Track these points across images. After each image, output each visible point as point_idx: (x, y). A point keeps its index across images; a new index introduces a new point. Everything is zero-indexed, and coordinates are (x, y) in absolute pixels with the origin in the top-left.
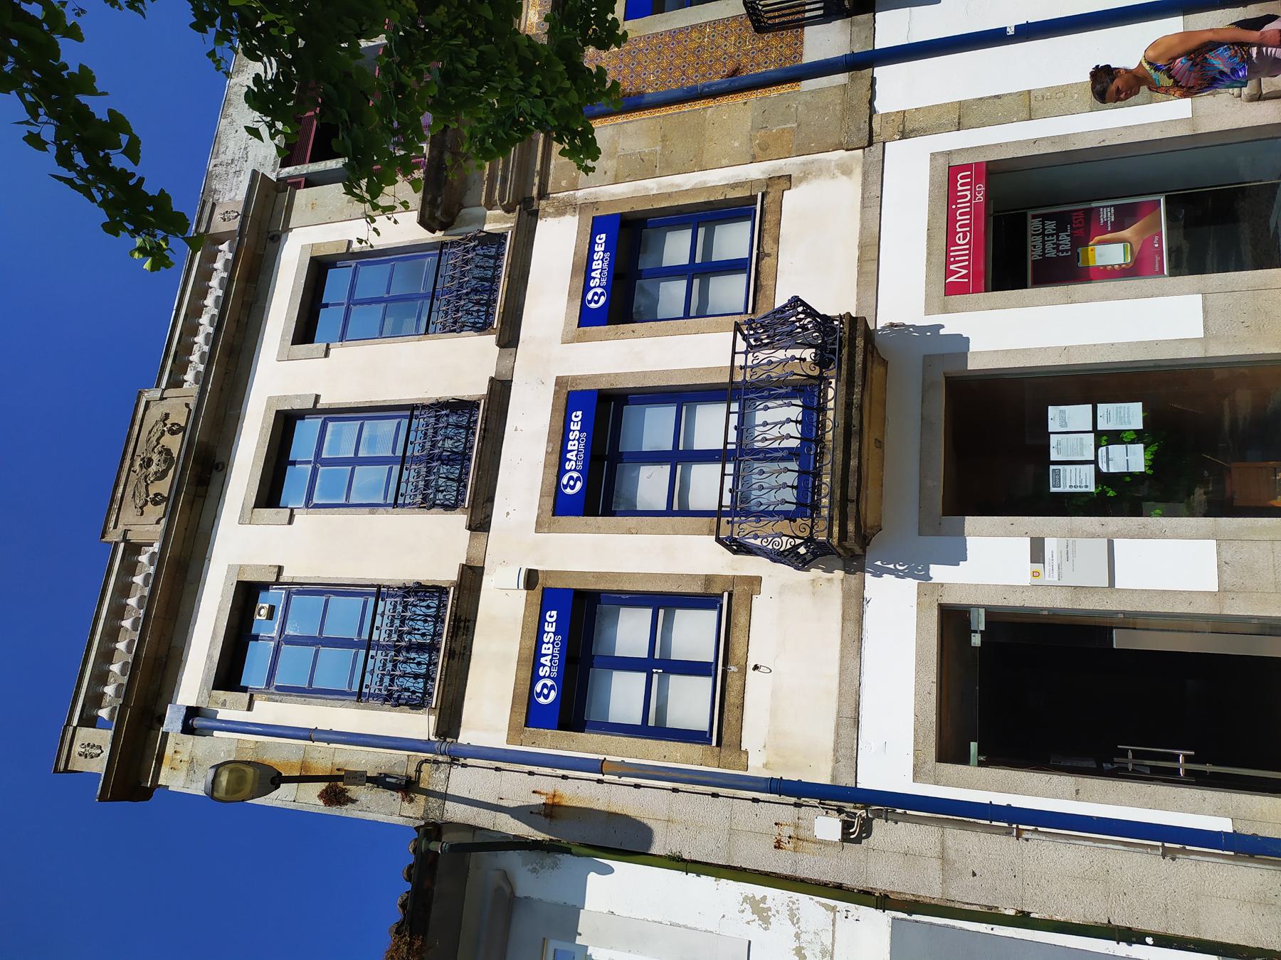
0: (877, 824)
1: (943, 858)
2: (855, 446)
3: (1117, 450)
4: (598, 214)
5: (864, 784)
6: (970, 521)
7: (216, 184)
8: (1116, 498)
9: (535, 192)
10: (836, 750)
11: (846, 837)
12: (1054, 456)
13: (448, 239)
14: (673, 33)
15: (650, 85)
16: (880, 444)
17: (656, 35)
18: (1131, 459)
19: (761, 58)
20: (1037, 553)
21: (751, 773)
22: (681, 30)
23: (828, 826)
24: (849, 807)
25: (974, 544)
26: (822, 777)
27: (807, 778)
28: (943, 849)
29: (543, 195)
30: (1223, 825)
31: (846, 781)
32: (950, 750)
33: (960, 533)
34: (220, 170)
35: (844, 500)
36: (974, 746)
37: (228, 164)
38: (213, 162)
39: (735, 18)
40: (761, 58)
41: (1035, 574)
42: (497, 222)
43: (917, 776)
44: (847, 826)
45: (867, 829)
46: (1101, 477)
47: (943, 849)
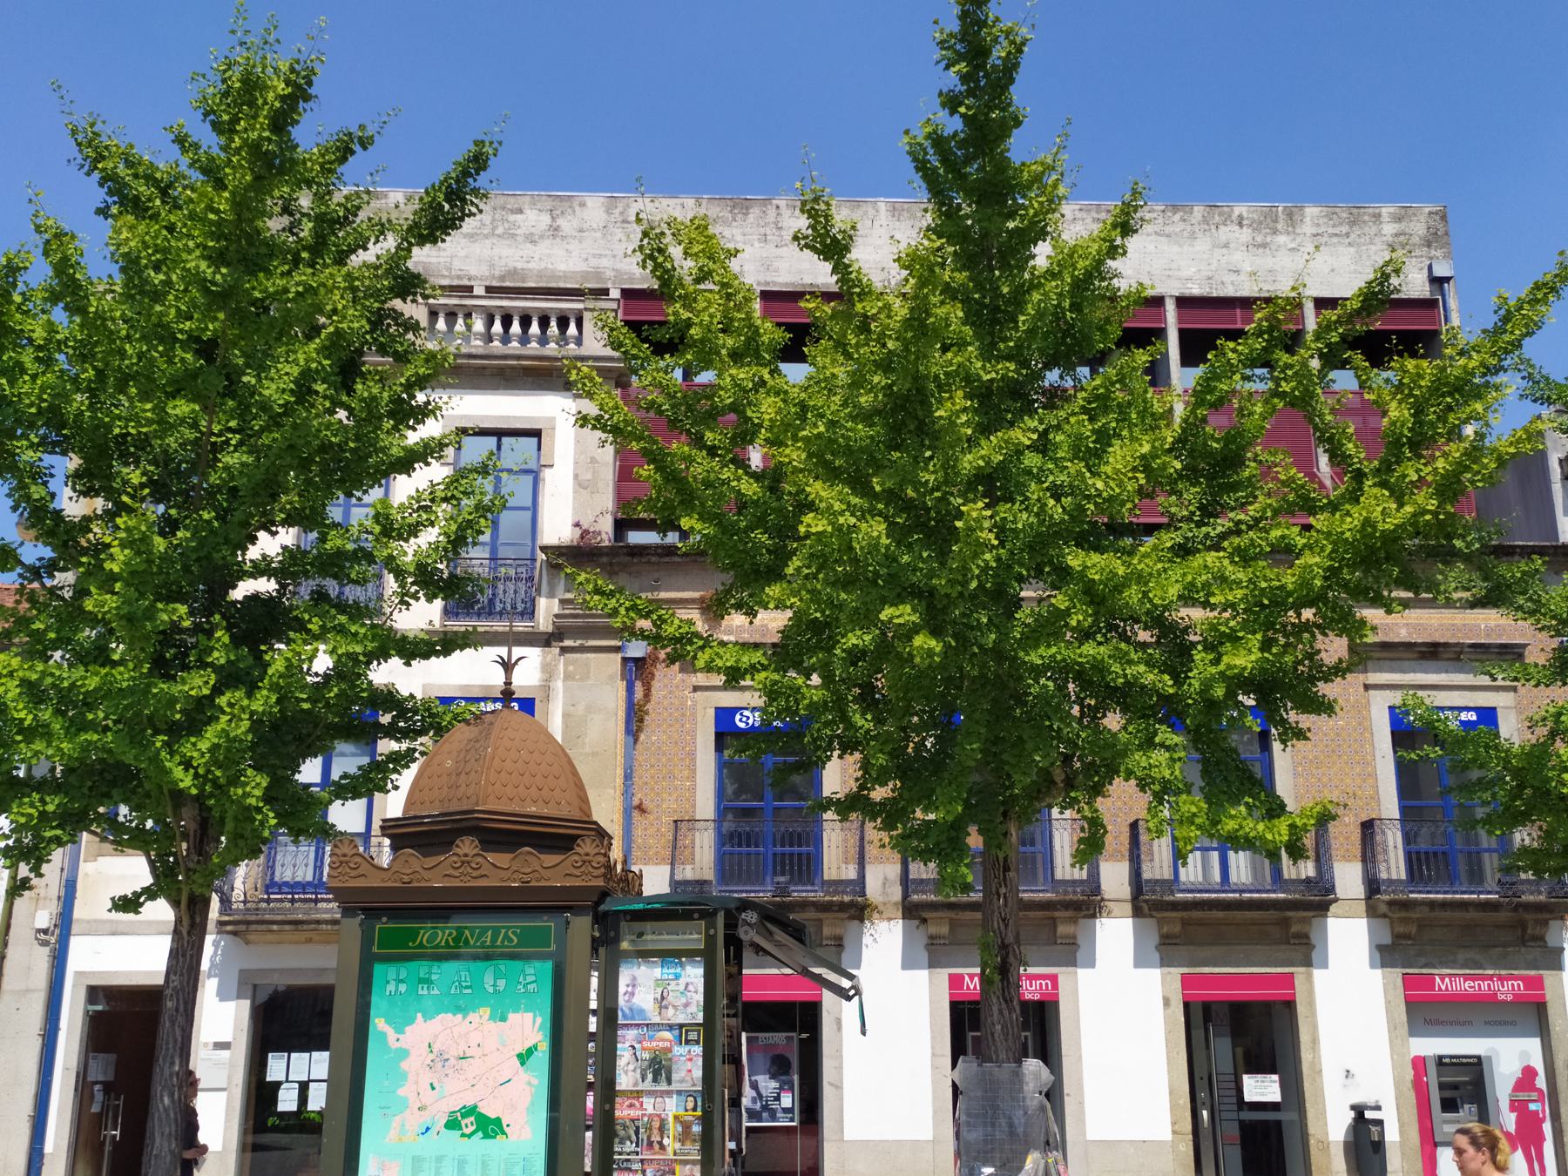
0: (46, 950)
1: (27, 991)
2: (287, 927)
3: (295, 1094)
4: (537, 702)
5: (74, 942)
6: (246, 1004)
7: (755, 212)
8: (260, 1094)
9: (567, 643)
10: (95, 921)
11: (39, 931)
12: (293, 1055)
13: (538, 564)
14: (692, 755)
15: (648, 737)
16: (309, 941)
17: (694, 738)
18: (287, 1101)
19: (651, 831)
20: (224, 1046)
21: (81, 864)
22: (693, 760)
23: (44, 919)
24: (57, 931)
25: (231, 1006)
26: (78, 913)
27: (77, 903)
28: (33, 991)
29: (564, 650)
30: (48, 1147)
31: (75, 928)
32: (94, 993)
33: (239, 997)
34: (772, 212)
35: (248, 923)
36: (100, 1008)
37: (776, 223)
38: (782, 204)
39: (694, 806)
40: (651, 831)
41: (206, 1044)
42: (547, 610)
43: (78, 974)
44: (45, 932)
45: (45, 943)
46: (278, 1085)
47: (33, 991)
